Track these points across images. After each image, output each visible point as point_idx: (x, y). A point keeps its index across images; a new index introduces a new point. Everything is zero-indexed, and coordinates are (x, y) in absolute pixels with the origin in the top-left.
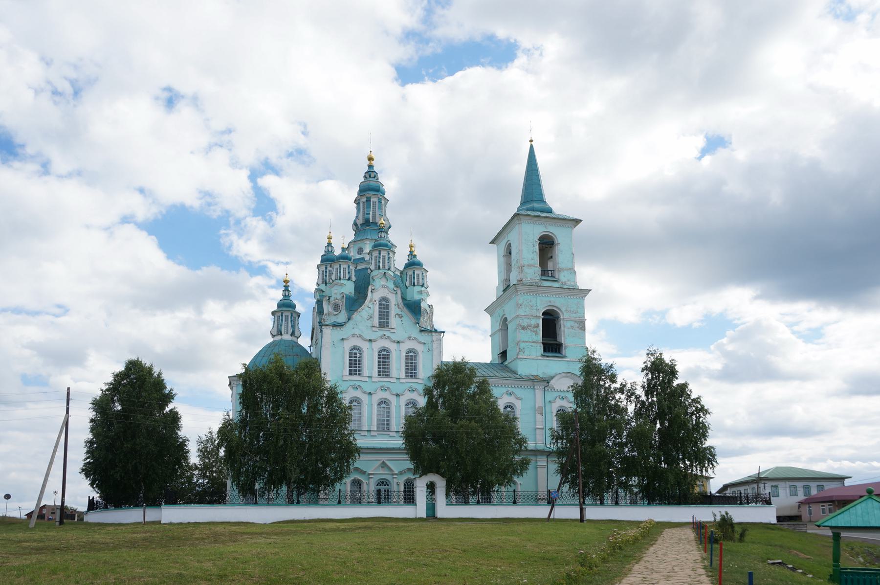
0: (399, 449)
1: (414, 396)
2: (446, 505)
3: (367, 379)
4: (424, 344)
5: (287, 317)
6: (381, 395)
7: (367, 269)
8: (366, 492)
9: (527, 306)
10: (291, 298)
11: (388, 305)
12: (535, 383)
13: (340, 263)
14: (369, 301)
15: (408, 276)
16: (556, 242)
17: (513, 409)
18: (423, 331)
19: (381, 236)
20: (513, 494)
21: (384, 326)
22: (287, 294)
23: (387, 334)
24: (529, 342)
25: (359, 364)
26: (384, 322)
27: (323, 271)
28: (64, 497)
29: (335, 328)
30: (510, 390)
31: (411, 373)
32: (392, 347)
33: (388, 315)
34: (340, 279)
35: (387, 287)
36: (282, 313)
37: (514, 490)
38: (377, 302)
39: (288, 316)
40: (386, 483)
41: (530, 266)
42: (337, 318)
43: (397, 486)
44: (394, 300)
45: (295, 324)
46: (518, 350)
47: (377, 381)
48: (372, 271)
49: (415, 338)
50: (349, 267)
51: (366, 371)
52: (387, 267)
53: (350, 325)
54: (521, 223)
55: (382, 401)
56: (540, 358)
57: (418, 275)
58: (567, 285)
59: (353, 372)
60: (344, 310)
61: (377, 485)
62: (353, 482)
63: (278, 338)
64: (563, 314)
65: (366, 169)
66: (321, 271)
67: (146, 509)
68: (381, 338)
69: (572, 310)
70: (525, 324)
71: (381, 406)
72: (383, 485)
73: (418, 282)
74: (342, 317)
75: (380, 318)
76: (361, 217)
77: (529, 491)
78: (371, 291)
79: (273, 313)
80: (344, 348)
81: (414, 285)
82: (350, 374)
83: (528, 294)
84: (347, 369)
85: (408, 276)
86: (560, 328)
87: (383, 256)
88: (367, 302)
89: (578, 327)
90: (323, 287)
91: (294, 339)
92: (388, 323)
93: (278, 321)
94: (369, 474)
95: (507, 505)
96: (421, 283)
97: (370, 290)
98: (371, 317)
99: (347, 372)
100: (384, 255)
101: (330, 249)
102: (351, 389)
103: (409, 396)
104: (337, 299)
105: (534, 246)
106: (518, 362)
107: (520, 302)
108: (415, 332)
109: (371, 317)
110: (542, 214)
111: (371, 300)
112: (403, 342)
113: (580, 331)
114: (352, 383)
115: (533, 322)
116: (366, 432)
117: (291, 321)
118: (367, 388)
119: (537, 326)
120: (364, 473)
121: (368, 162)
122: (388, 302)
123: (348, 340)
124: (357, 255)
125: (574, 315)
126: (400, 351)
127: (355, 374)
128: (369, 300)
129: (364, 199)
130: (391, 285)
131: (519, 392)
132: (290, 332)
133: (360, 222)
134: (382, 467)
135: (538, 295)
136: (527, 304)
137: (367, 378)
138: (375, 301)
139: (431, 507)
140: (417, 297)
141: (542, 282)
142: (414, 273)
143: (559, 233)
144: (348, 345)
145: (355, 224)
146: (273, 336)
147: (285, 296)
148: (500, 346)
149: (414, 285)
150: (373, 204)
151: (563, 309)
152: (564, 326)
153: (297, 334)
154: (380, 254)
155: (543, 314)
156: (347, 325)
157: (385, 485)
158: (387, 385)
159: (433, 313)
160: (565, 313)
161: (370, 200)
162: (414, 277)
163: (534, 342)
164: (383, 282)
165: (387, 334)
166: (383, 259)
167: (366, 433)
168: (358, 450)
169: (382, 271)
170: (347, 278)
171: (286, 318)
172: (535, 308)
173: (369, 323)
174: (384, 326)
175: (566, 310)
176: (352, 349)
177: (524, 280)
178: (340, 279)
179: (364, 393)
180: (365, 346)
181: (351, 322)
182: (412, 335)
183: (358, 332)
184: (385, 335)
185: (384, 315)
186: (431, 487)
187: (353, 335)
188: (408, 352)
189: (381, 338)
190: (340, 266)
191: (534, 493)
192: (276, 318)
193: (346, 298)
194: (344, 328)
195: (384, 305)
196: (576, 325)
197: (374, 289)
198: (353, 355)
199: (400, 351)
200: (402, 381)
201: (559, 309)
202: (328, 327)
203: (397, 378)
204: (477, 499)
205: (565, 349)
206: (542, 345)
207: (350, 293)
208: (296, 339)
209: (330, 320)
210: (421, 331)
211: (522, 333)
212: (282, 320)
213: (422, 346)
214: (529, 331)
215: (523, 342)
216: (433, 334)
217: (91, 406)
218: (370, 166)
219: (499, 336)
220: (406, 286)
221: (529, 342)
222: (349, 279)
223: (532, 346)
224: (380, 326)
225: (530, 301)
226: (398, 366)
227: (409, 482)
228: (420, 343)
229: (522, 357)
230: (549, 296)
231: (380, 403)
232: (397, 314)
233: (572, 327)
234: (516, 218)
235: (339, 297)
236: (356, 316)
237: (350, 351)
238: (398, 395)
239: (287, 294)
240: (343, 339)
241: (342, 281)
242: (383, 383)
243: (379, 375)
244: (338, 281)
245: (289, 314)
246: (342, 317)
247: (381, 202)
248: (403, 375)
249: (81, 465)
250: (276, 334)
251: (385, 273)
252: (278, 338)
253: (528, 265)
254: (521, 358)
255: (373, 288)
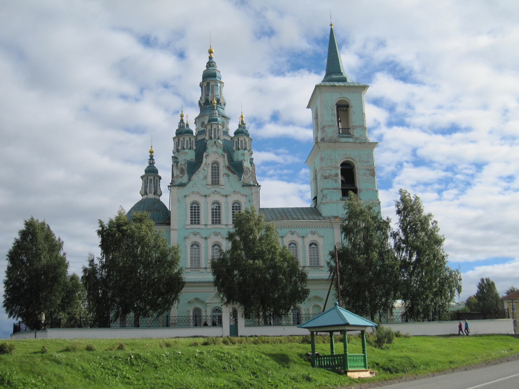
0: (209, 282)
1: (218, 239)
2: (245, 326)
3: (203, 227)
4: (246, 196)
5: (151, 180)
6: (193, 239)
7: (204, 139)
8: (304, 315)
9: (328, 159)
10: (155, 165)
11: (218, 167)
12: (333, 223)
13: (184, 136)
14: (204, 165)
15: (235, 142)
16: (350, 105)
17: (296, 245)
18: (245, 185)
19: (213, 113)
20: (166, 319)
21: (215, 184)
22: (151, 162)
23: (218, 190)
24: (331, 189)
25: (219, 215)
26: (215, 182)
27: (176, 142)
28: (231, 326)
29: (179, 188)
30: (314, 230)
31: (216, 220)
32: (222, 200)
33: (218, 175)
34: (184, 149)
35: (217, 153)
36: (147, 177)
37: (167, 316)
38: (210, 165)
39: (152, 179)
40: (220, 310)
41: (330, 126)
42: (182, 180)
43: (207, 313)
44: (223, 162)
45: (157, 185)
46: (322, 196)
47: (189, 228)
48: (207, 141)
49: (238, 192)
50: (190, 139)
51: (202, 221)
52: (217, 138)
53: (190, 185)
54: (322, 92)
55: (215, 244)
56: (340, 202)
57: (242, 141)
58: (359, 140)
59: (215, 222)
60: (186, 173)
61: (213, 312)
62: (195, 310)
63: (145, 197)
64: (357, 163)
65: (207, 60)
66: (175, 142)
67: (37, 332)
68: (214, 193)
69: (364, 160)
70: (327, 174)
71: (215, 248)
72: (217, 312)
73: (242, 146)
74: (185, 179)
75: (212, 178)
76: (203, 98)
77: (186, 316)
78: (206, 157)
79: (142, 177)
80: (186, 203)
81: (239, 149)
82: (192, 223)
83: (329, 150)
84: (189, 219)
85: (235, 142)
86: (356, 175)
87: (214, 129)
88: (203, 165)
89: (369, 174)
90: (177, 154)
91: (157, 197)
92: (218, 181)
93: (145, 184)
94: (206, 304)
95: (130, 327)
96: (244, 148)
97: (204, 156)
98: (205, 178)
99: (189, 222)
100: (214, 127)
101: (182, 124)
102: (192, 236)
103: (214, 239)
104: (182, 165)
105: (332, 110)
106: (322, 205)
107: (322, 156)
108: (238, 187)
109: (205, 178)
110: (337, 84)
111: (206, 164)
112: (230, 195)
113: (371, 177)
114: (192, 230)
115: (333, 172)
116: (204, 269)
117: (154, 183)
118: (204, 234)
119: (337, 175)
120: (202, 302)
121: (150, 154)
122: (219, 165)
123: (189, 196)
124: (201, 128)
125: (366, 164)
126: (228, 203)
127: (195, 223)
128: (204, 164)
129: (205, 84)
130: (220, 151)
131: (321, 231)
132: (153, 192)
133: (203, 102)
134: (216, 297)
135: (336, 150)
136: (328, 158)
137: (204, 226)
138: (209, 164)
139: (234, 330)
140: (240, 158)
141: (339, 139)
142: (238, 140)
143: (350, 97)
144: (189, 201)
145: (200, 104)
146: (142, 195)
147: (150, 164)
148: (315, 192)
149: (239, 149)
150: (212, 87)
151: (357, 160)
152: (358, 174)
153: (159, 193)
154: (212, 127)
155: (342, 165)
156: (189, 185)
157: (219, 312)
158: (218, 230)
159: (255, 170)
160: (358, 163)
161: (209, 85)
162: (238, 143)
163: (334, 189)
164: (214, 149)
165: (218, 190)
166: (214, 131)
167: (203, 270)
168: (184, 283)
169: (213, 140)
170: (189, 148)
171: (150, 181)
172: (334, 161)
173: (204, 182)
174: (215, 184)
175: (359, 161)
176: (192, 203)
177: (325, 138)
178: (184, 149)
179: (202, 238)
180: (202, 201)
181: (191, 183)
182: (236, 190)
183: (195, 189)
184: (216, 191)
185: (215, 175)
186: (234, 314)
187: (193, 193)
188: (234, 204)
189: (214, 193)
190: (184, 139)
191: (176, 317)
192: (144, 181)
193: (187, 163)
194: (186, 188)
195: (215, 167)
196: (368, 172)
197: (207, 155)
198: (193, 208)
199: (228, 203)
200: (209, 227)
201: (353, 160)
202: (174, 187)
203: (226, 225)
204: (166, 323)
205: (360, 192)
206: (341, 191)
207: (192, 159)
208: (158, 196)
209: (178, 181)
210: (243, 186)
211: (325, 182)
212: (147, 183)
213: (244, 198)
214: (330, 180)
215: (326, 189)
216: (253, 187)
217: (7, 257)
218: (210, 58)
219: (313, 184)
220: (233, 150)
221: (331, 189)
222: (190, 149)
223: (333, 192)
224: (213, 184)
225: (330, 155)
226: (206, 216)
227: (197, 310)
228: (242, 195)
229: (325, 202)
230: (345, 150)
231: (214, 245)
232: (226, 174)
233: (365, 174)
234: (317, 89)
235: (183, 163)
236: (194, 177)
237: (191, 205)
238: (206, 238)
239: (151, 162)
240: (185, 196)
241: (186, 151)
242: (195, 230)
243: (213, 223)
244: (183, 151)
245: (152, 178)
246: (185, 179)
247: (218, 86)
248: (210, 222)
249: (515, 287)
250: (143, 194)
251: (215, 142)
252: (145, 197)
253: (328, 126)
254: (324, 203)
255: (207, 154)
